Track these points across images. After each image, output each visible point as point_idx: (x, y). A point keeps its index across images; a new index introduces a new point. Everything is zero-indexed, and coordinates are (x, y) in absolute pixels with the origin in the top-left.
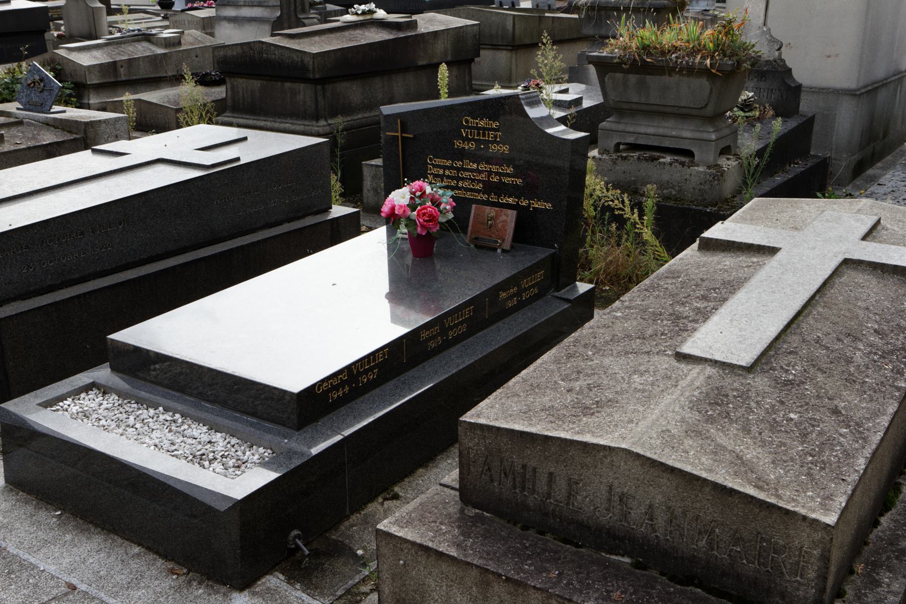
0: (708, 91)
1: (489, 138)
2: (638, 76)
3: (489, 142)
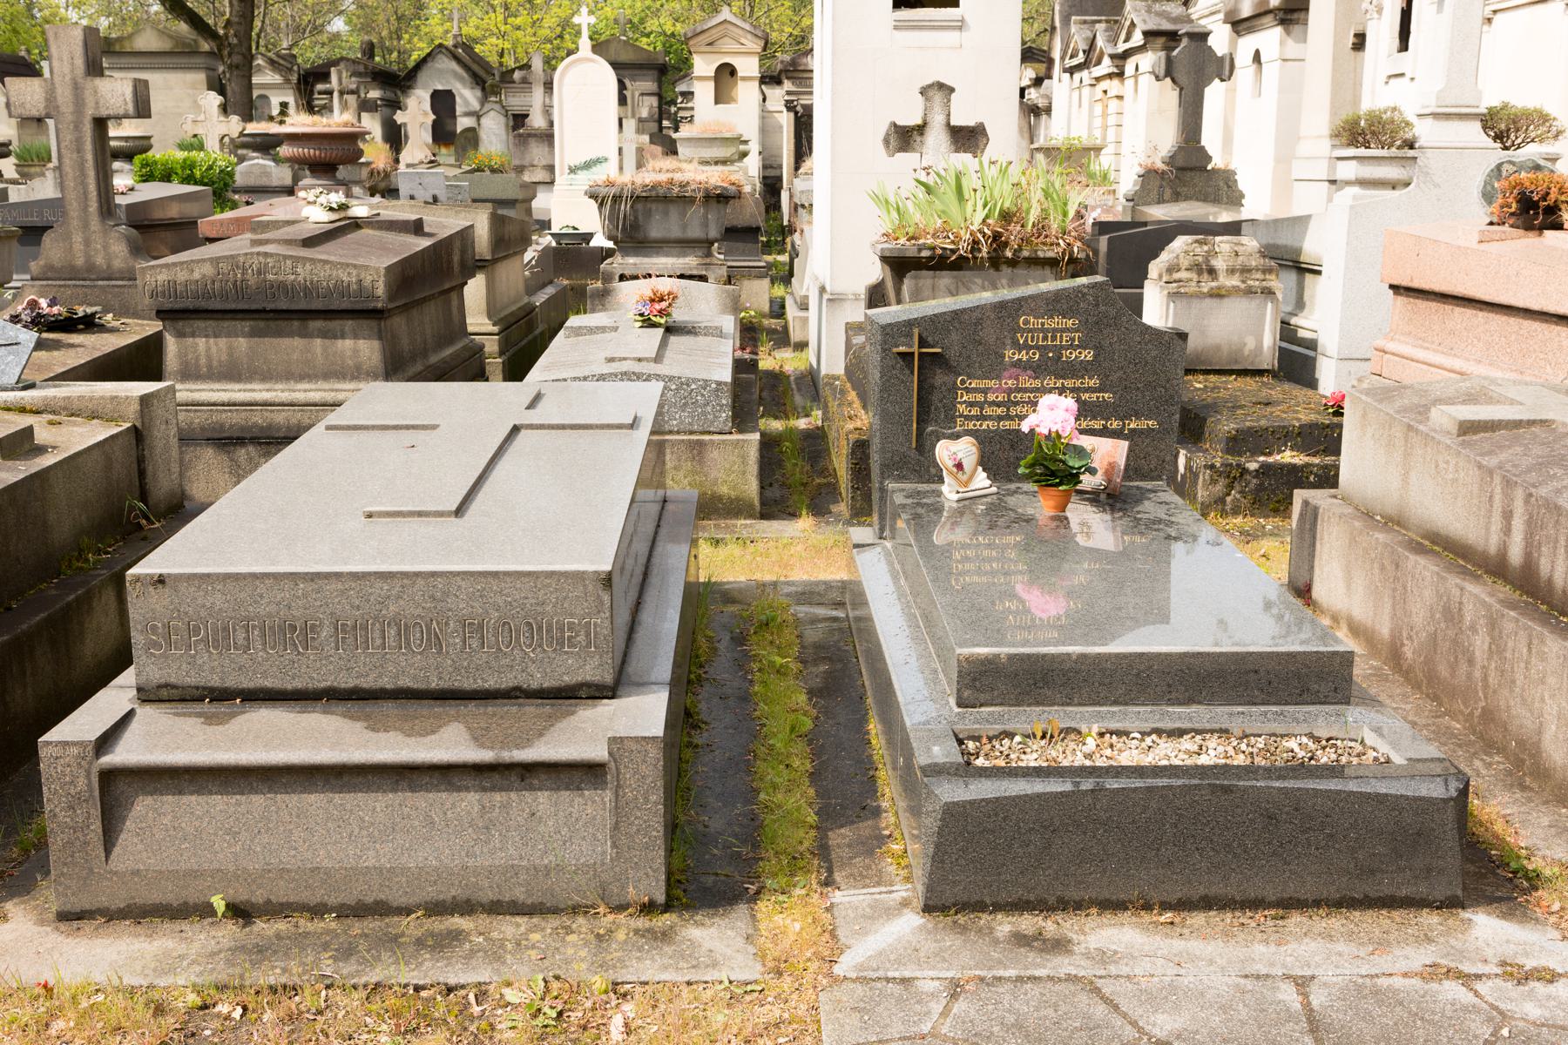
3: (1062, 347)
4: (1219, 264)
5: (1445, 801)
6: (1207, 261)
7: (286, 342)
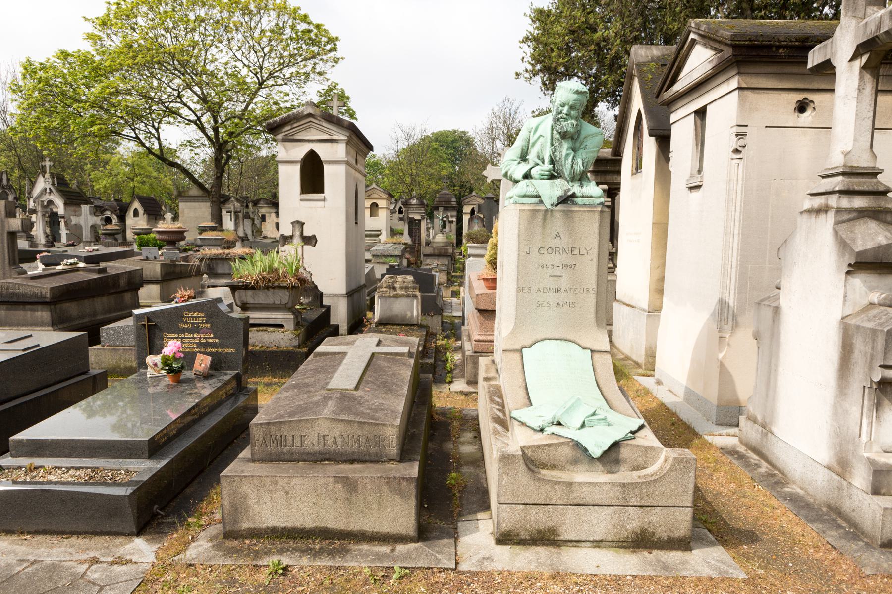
4: (397, 285)
5: (125, 496)
6: (393, 284)
7: (18, 313)
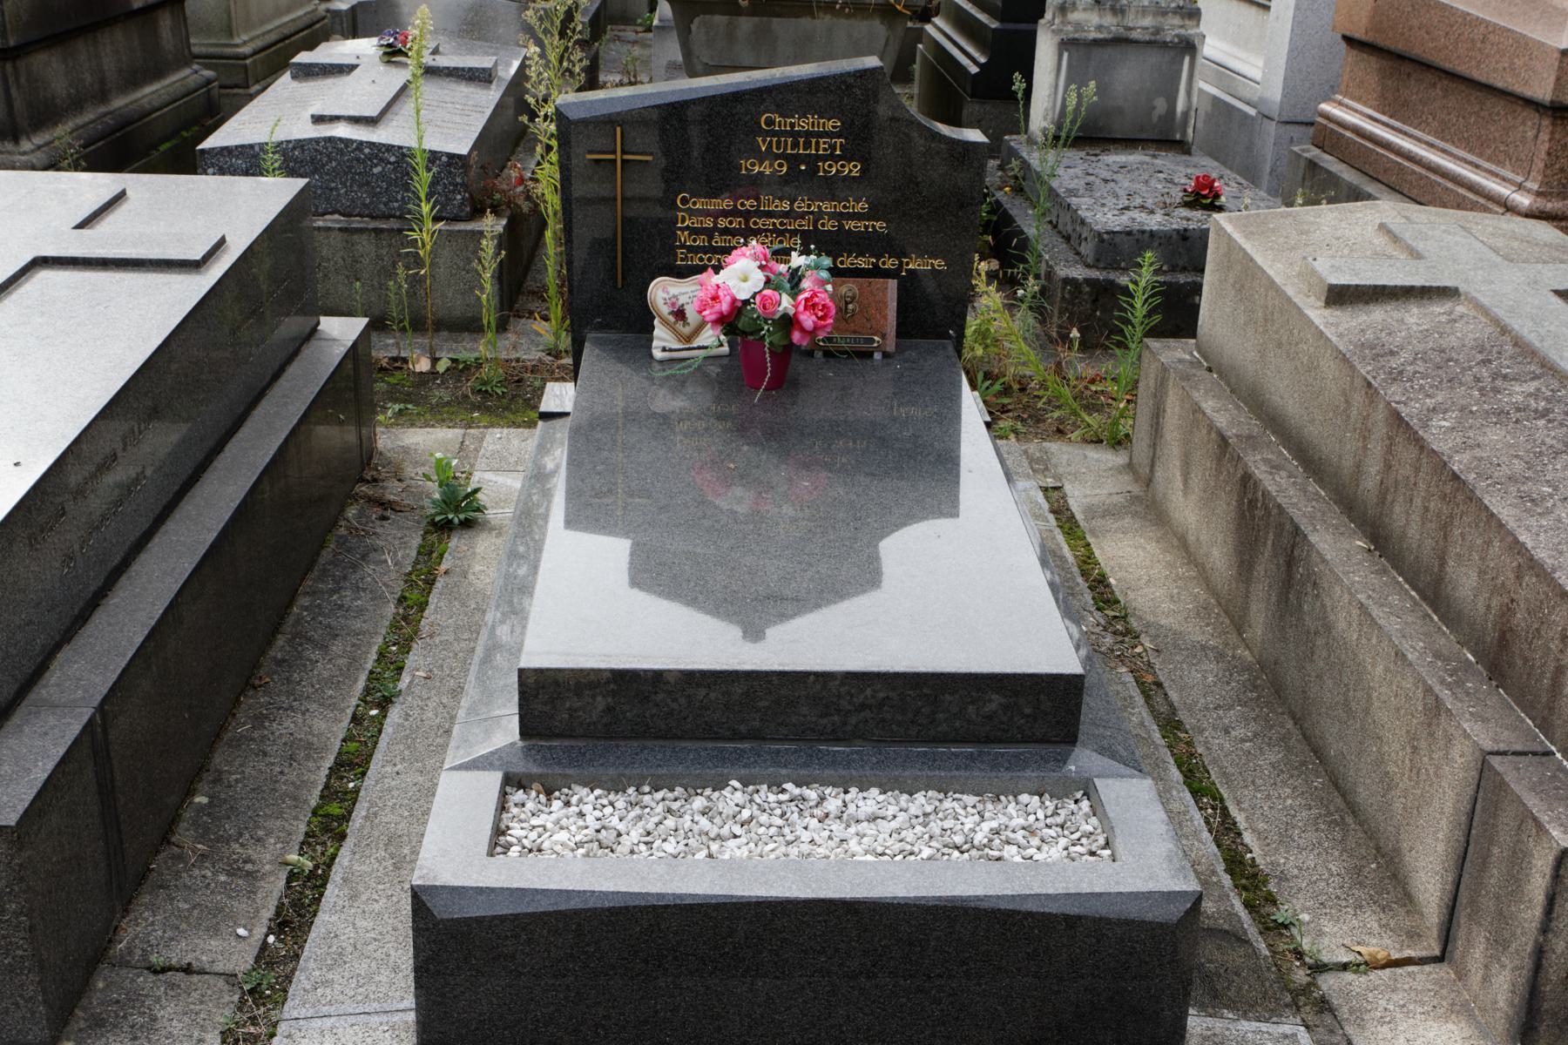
0: (883, 42)
1: (817, 150)
2: (756, 19)
3: (819, 158)
